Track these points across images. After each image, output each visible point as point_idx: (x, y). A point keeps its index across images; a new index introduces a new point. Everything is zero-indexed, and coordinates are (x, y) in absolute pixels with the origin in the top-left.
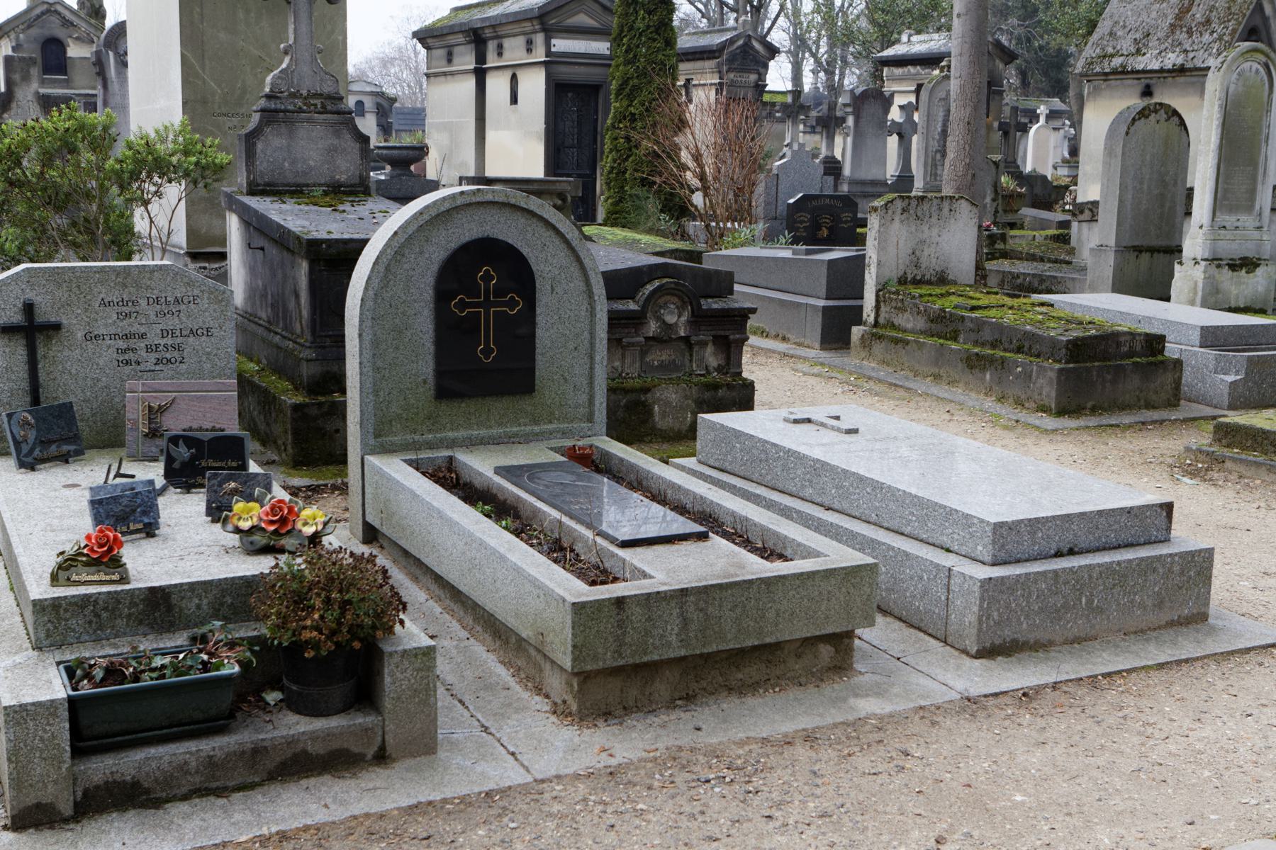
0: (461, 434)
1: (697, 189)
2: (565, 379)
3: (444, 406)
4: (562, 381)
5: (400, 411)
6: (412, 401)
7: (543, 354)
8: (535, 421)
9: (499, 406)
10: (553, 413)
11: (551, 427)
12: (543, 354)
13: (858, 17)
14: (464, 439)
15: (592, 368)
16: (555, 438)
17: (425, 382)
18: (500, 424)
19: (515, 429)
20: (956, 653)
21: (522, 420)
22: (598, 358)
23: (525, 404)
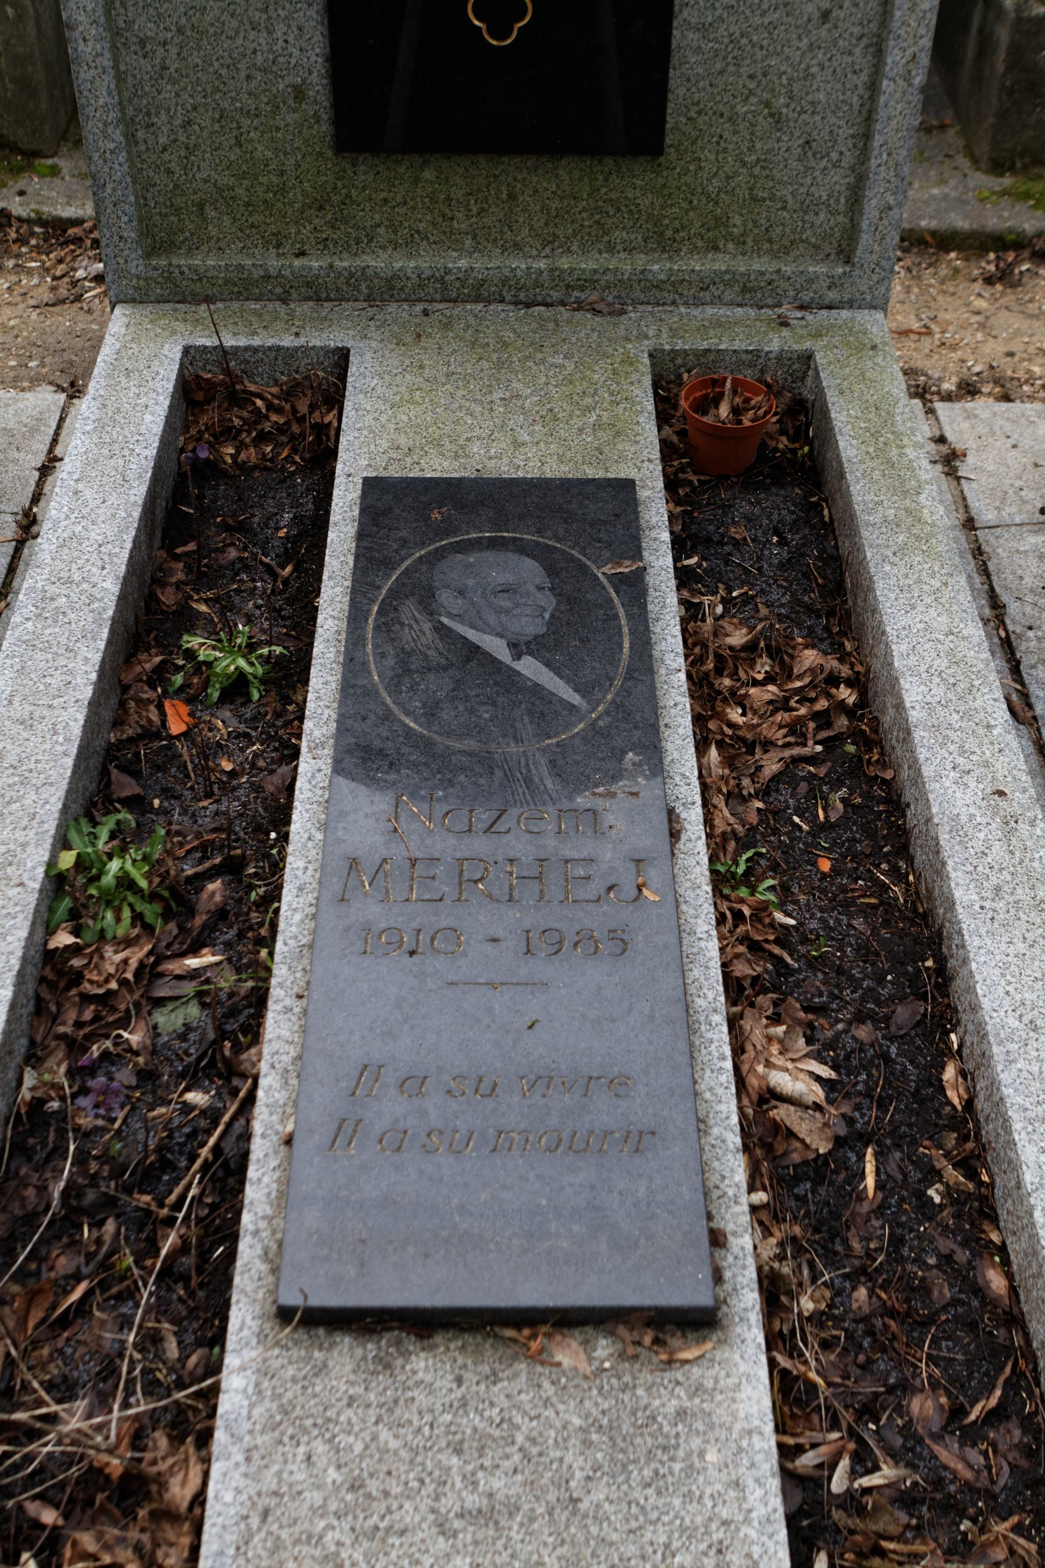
0: (419, 262)
1: (177, 737)
2: (776, 117)
3: (364, 174)
4: (764, 123)
5: (225, 180)
6: (263, 152)
7: (703, 29)
8: (665, 242)
9: (547, 184)
10: (723, 221)
11: (719, 263)
12: (703, 29)
13: (163, 714)
14: (423, 281)
15: (873, 88)
16: (718, 300)
17: (299, 93)
18: (549, 242)
19: (588, 264)
20: (994, 578)
21: (619, 235)
22: (895, 58)
23: (634, 184)
